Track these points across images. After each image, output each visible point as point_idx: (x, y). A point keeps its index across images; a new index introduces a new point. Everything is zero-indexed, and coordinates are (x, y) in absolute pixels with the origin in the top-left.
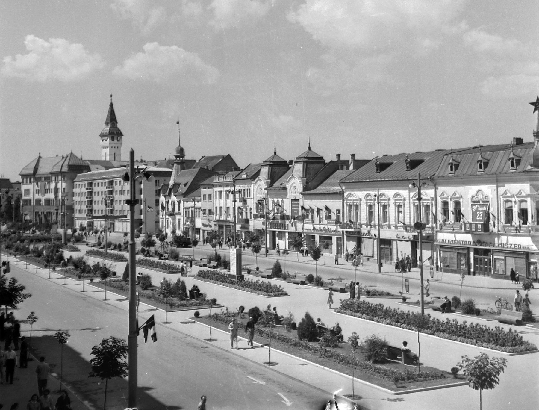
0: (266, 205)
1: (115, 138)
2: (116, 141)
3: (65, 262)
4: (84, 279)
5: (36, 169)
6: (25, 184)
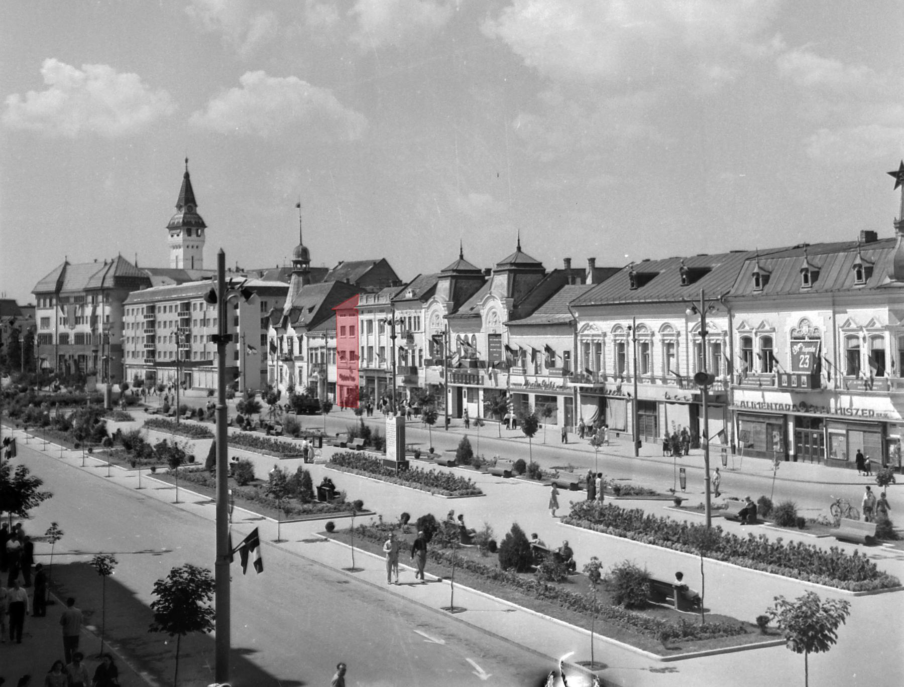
1: (194, 231)
2: (194, 236)
5: (60, 283)
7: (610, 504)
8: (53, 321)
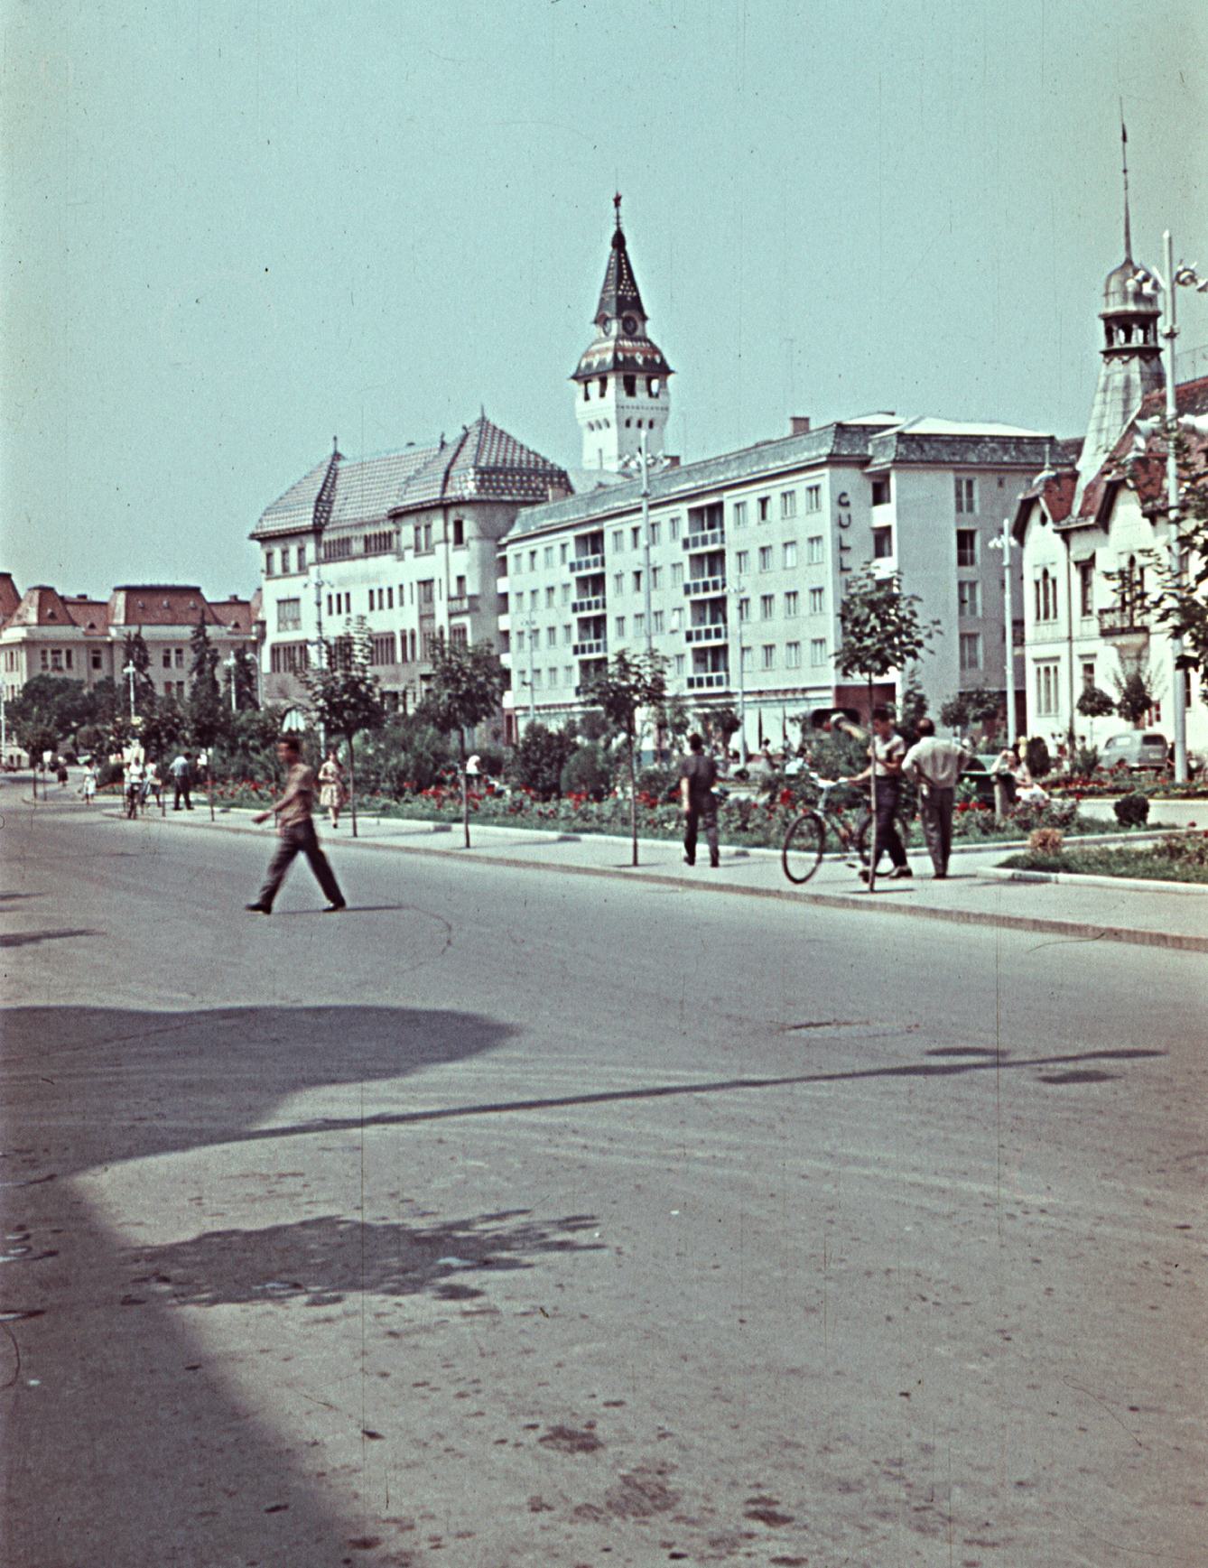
0: (688, 1159)
1: (640, 383)
2: (642, 395)
5: (323, 503)
6: (278, 578)
8: (308, 611)
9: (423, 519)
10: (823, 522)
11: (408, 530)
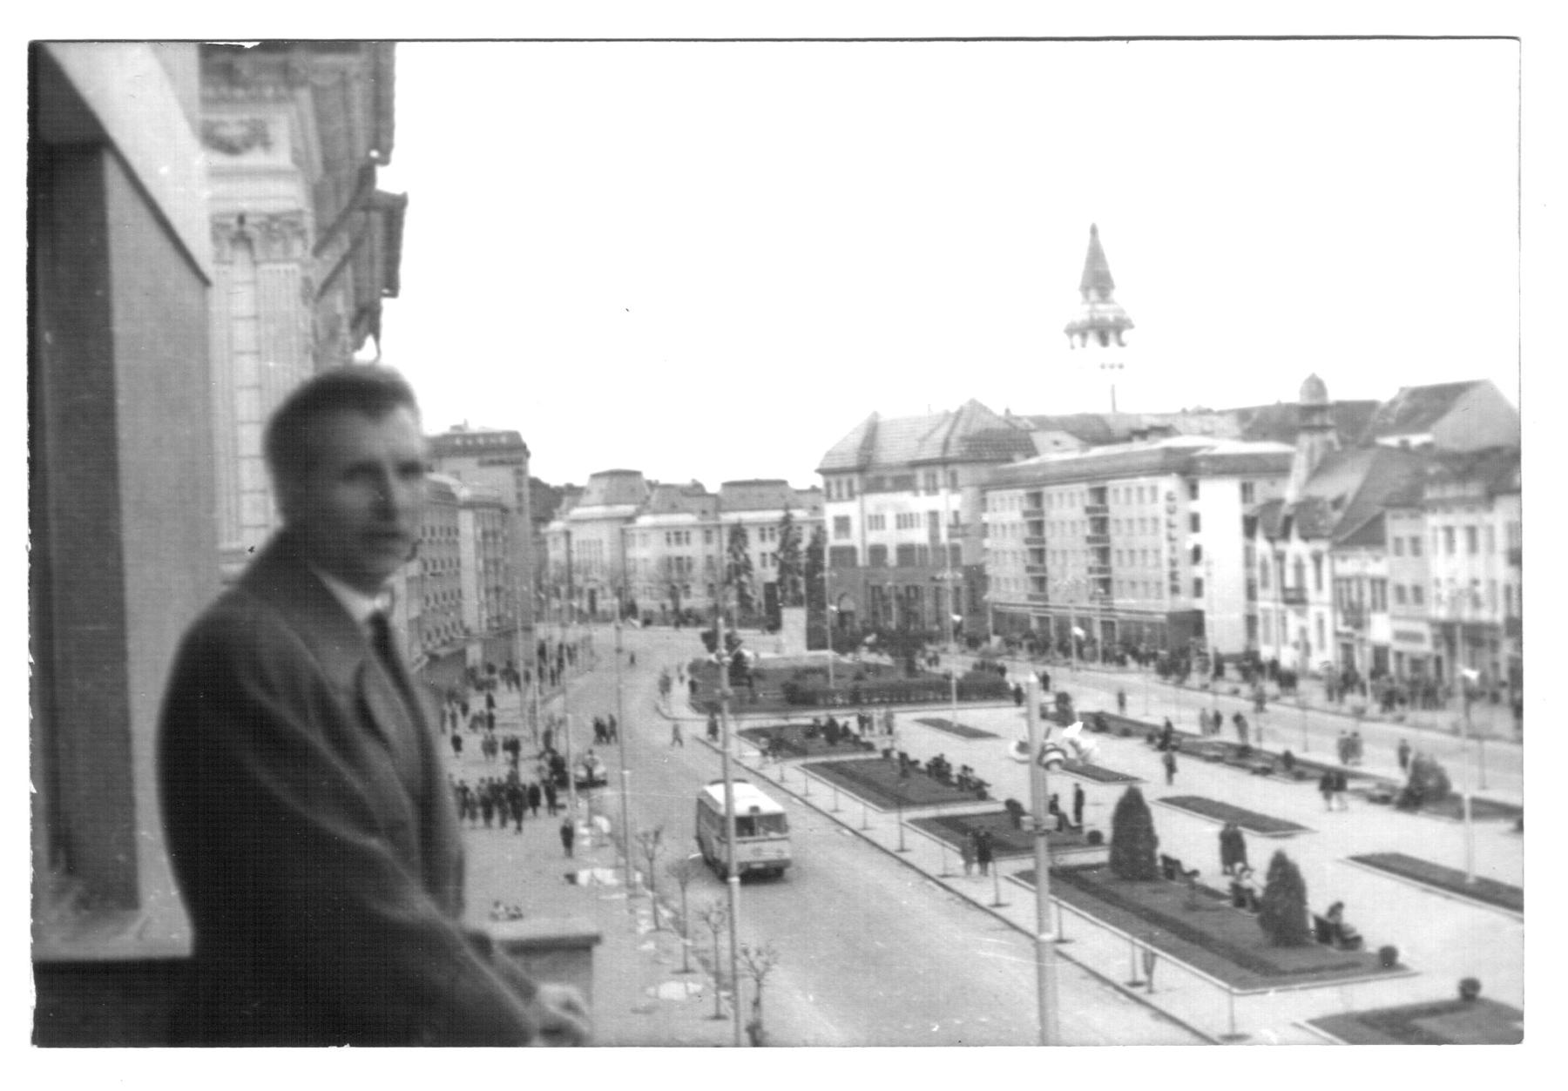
3: (1053, 847)
4: (940, 806)
7: (1169, 725)
8: (855, 525)
9: (931, 469)
10: (1160, 509)
11: (920, 474)
